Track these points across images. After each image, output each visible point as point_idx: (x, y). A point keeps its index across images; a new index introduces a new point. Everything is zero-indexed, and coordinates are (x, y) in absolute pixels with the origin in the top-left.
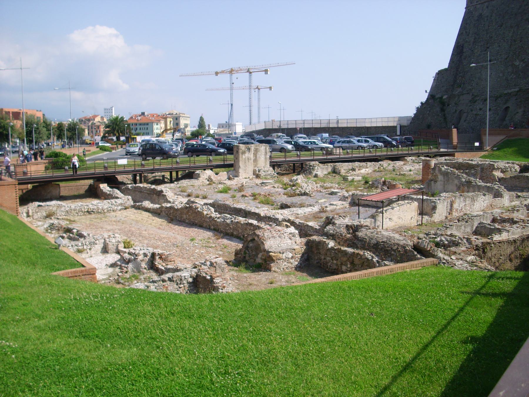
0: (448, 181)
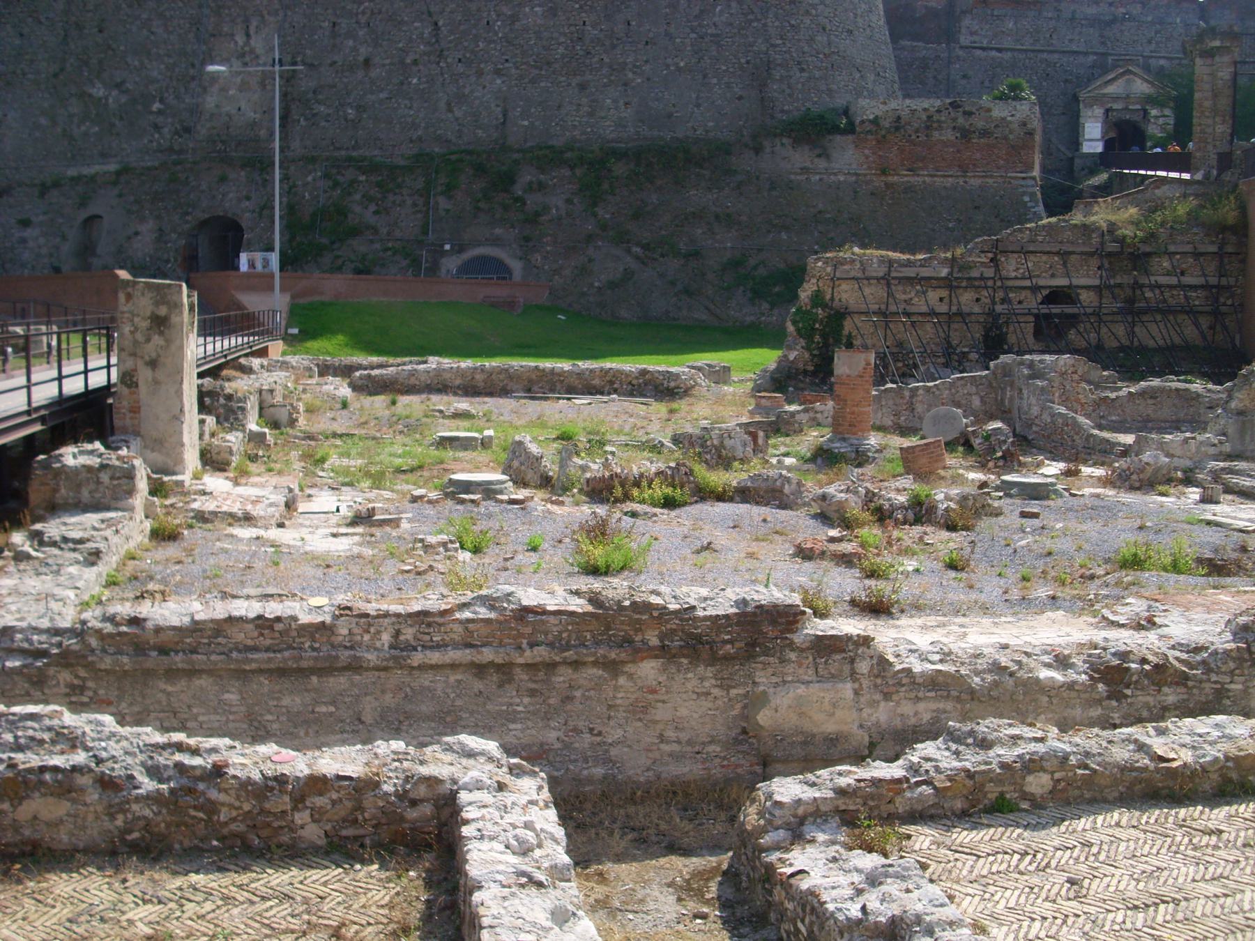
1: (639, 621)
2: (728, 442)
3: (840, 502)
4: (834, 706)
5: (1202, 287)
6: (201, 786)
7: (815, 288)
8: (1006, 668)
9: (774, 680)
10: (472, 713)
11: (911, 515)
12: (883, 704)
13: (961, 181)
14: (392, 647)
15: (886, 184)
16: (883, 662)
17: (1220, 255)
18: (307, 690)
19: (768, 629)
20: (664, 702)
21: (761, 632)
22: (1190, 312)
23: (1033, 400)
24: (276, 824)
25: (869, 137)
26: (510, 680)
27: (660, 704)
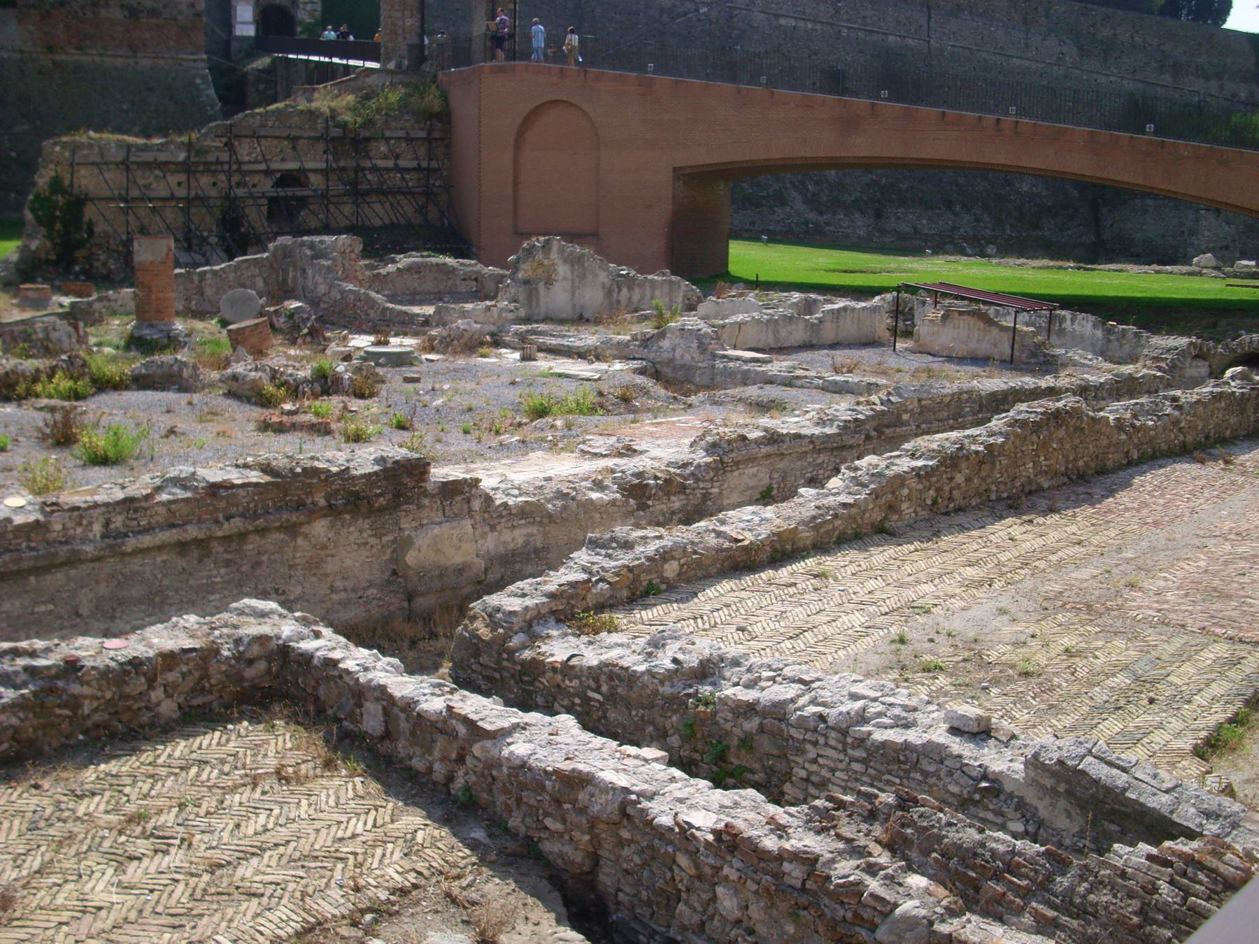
0: (583, 277)
1: (310, 485)
2: (54, 335)
3: (254, 380)
4: (460, 540)
5: (414, 169)
6: (61, 684)
7: (53, 174)
8: (568, 494)
9: (414, 524)
10: (177, 591)
11: (318, 388)
12: (490, 535)
13: (131, 61)
14: (103, 537)
15: (54, 63)
16: (488, 499)
17: (429, 140)
18: (26, 592)
19: (406, 480)
20: (333, 556)
21: (401, 484)
22: (406, 193)
23: (319, 279)
24: (136, 706)
25: (33, 11)
26: (208, 555)
27: (329, 559)
